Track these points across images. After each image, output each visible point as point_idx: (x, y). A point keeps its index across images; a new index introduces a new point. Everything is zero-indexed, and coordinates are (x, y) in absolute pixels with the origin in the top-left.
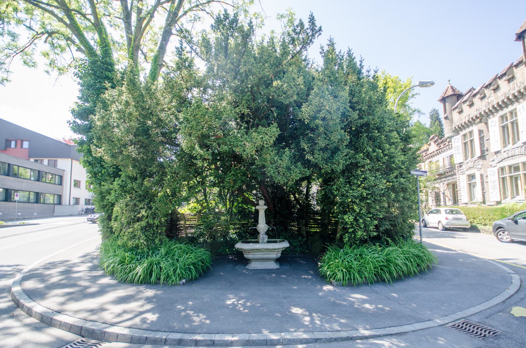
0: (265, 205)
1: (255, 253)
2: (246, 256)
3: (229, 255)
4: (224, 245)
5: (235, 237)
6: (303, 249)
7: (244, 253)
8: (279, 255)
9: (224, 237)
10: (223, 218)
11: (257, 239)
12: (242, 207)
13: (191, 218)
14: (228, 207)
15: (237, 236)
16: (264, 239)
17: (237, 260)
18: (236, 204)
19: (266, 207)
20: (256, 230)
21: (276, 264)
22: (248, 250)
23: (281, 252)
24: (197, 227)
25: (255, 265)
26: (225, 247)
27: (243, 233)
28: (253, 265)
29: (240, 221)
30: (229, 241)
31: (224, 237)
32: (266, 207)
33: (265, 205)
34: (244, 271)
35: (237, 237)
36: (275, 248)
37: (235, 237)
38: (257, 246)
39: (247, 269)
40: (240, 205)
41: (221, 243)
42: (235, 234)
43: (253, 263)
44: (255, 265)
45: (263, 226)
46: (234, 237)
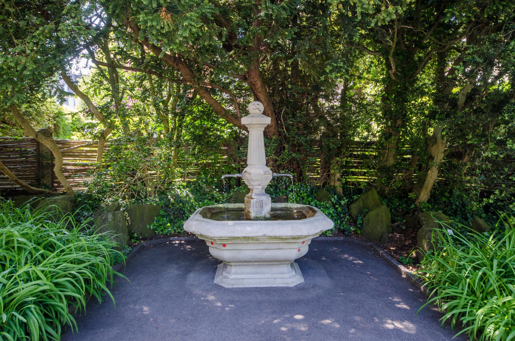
0: (264, 113)
1: (240, 247)
2: (215, 252)
3: (174, 235)
4: (162, 212)
5: (187, 195)
6: (341, 222)
7: (209, 244)
8: (305, 250)
9: (162, 193)
10: (157, 151)
11: (243, 202)
12: (201, 126)
13: (87, 151)
14: (171, 126)
15: (192, 191)
16: (262, 207)
17: (191, 252)
18: (188, 119)
19: (268, 120)
20: (239, 182)
21: (294, 273)
22: (221, 239)
23: (309, 243)
24: (99, 171)
25: (239, 276)
26: (163, 216)
27: (204, 186)
28: (233, 276)
29: (197, 159)
30: (173, 204)
31: (162, 193)
32: (268, 120)
33: (264, 113)
34: (211, 298)
35: (191, 196)
36: (299, 234)
37: (187, 195)
38: (248, 229)
39: (219, 287)
40: (197, 123)
41: (155, 210)
42: (187, 187)
43: (233, 270)
44: (239, 276)
45: (262, 171)
46: (184, 194)
